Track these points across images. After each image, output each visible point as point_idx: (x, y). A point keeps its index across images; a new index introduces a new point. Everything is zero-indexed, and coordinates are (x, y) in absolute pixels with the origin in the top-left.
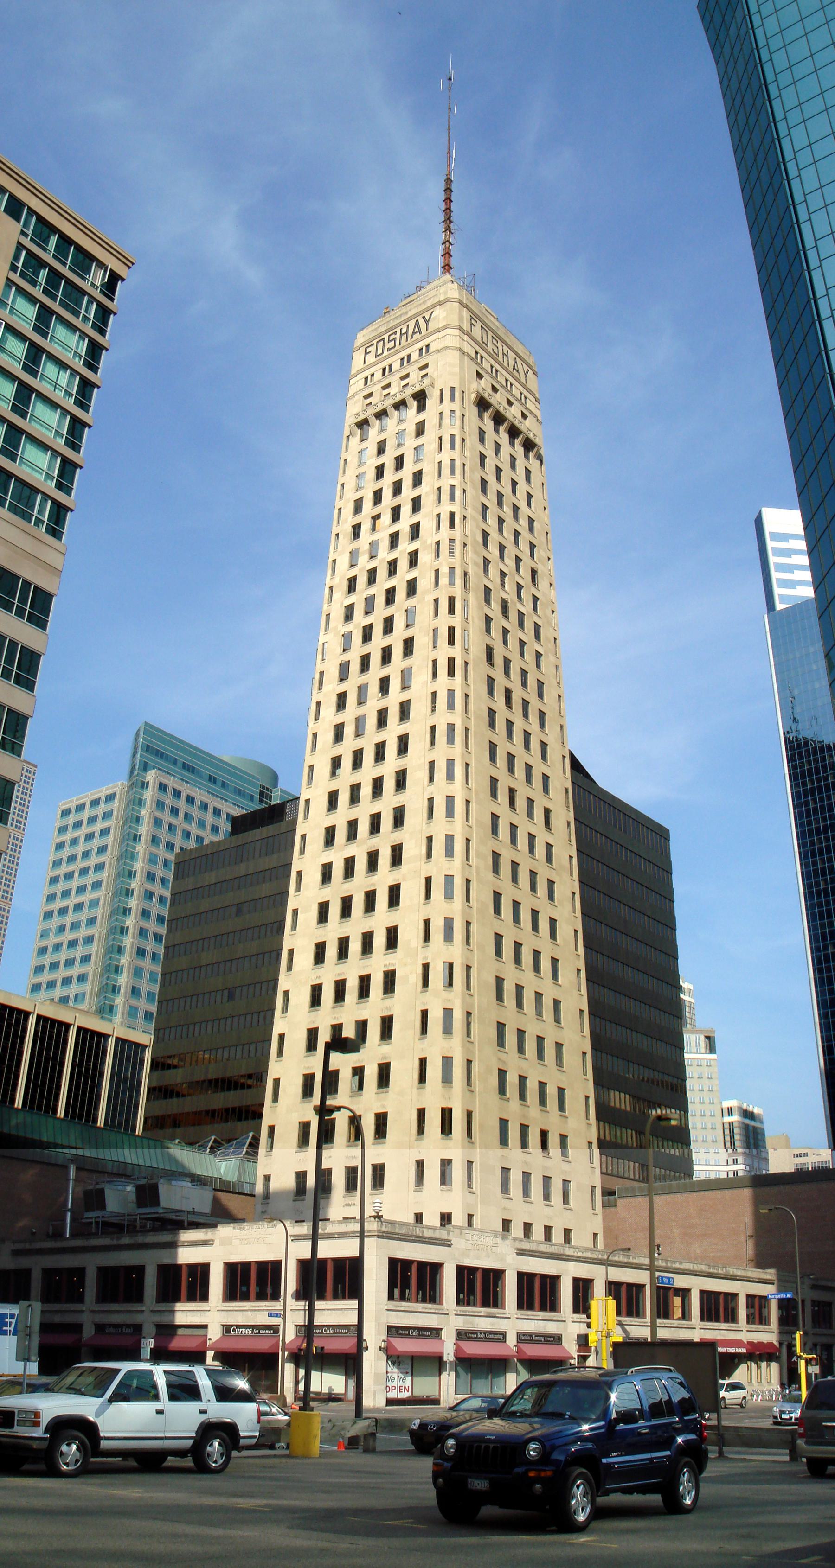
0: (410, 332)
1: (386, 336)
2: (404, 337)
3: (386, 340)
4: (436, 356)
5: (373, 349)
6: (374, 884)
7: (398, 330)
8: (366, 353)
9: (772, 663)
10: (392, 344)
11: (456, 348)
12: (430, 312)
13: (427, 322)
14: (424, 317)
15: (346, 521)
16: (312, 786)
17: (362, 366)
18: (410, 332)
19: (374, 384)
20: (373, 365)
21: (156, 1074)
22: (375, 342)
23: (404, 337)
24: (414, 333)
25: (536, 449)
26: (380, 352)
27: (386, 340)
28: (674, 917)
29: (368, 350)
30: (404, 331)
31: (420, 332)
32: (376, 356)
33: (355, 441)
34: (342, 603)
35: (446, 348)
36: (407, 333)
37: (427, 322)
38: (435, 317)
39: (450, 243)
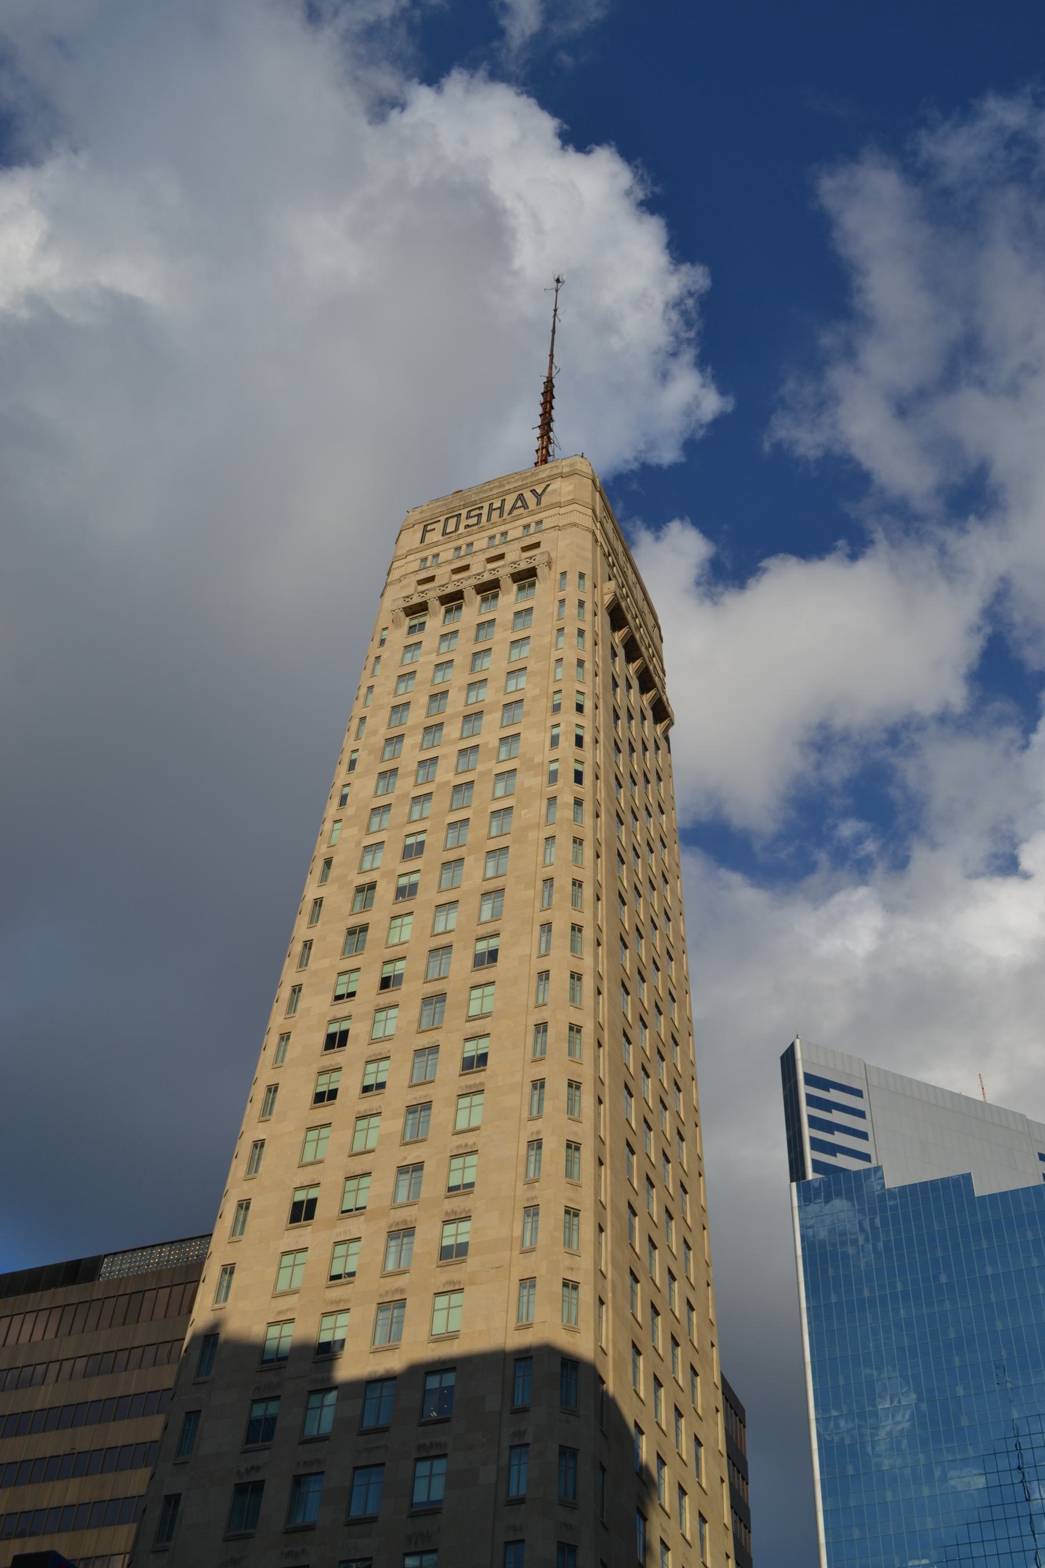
0: (508, 507)
1: (464, 512)
2: (495, 514)
3: (464, 516)
4: (553, 534)
5: (439, 527)
6: (401, 1291)
7: (486, 505)
8: (425, 531)
9: (795, 1203)
10: (474, 520)
11: (588, 529)
12: (544, 485)
14: (533, 491)
15: (375, 732)
16: (273, 1118)
17: (417, 543)
18: (508, 507)
19: (439, 565)
20: (436, 544)
21: (813, 1208)
22: (442, 519)
24: (514, 508)
25: (666, 722)
27: (464, 516)
28: (748, 1510)
29: (429, 528)
30: (497, 504)
31: (525, 506)
32: (444, 534)
33: (398, 637)
34: (359, 843)
35: (575, 525)
36: (501, 508)
37: (539, 497)
38: (554, 491)
39: (548, 452)
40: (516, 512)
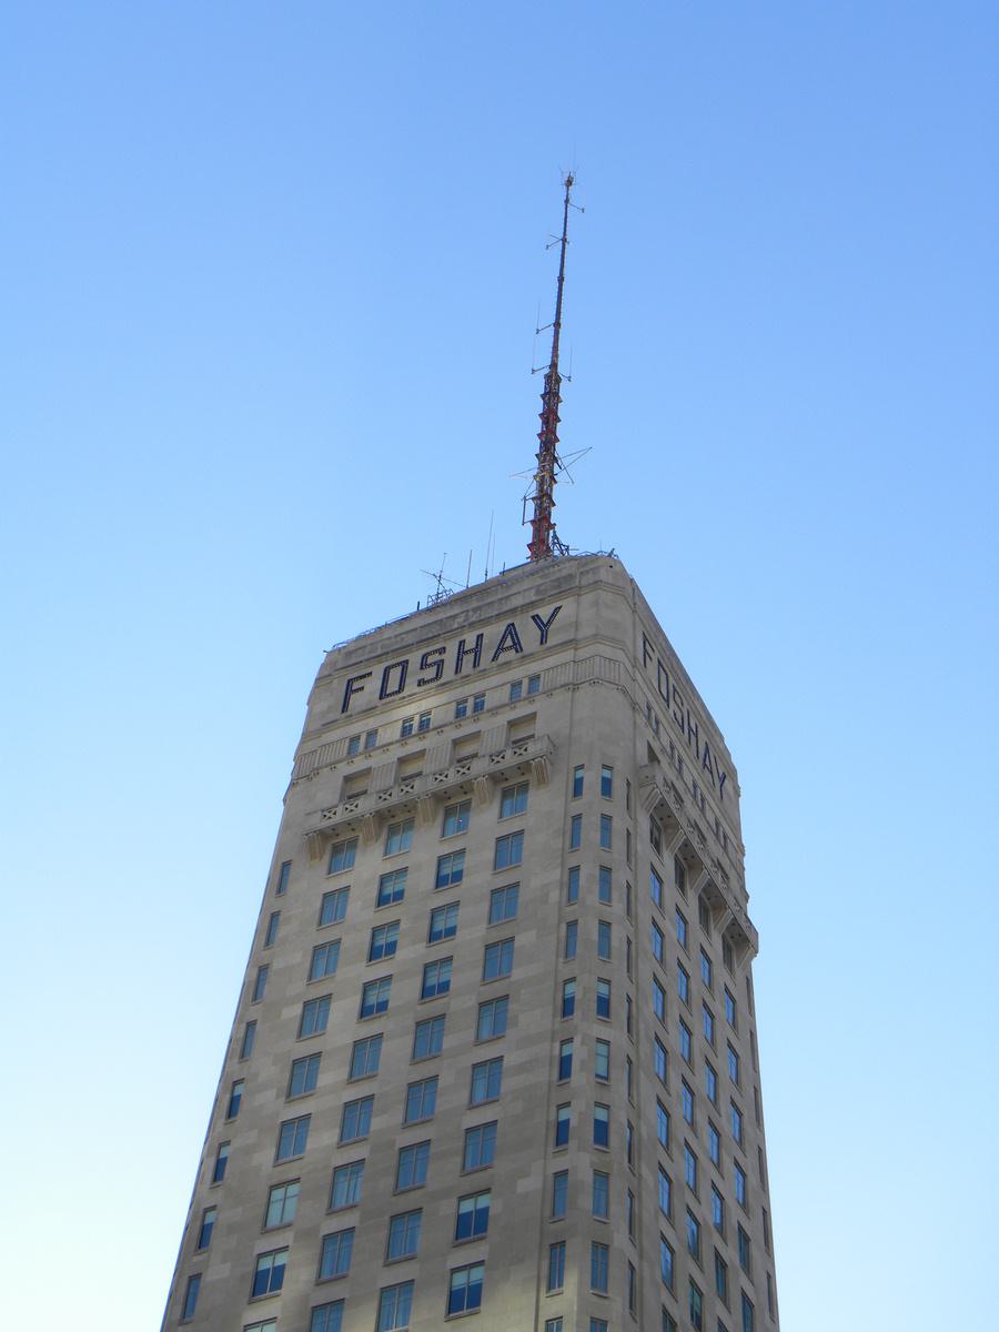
2: (468, 659)
10: (430, 673)
13: (543, 627)
20: (369, 711)
23: (468, 659)
24: (500, 649)
26: (393, 686)
31: (517, 646)
32: (404, 664)
40: (503, 657)
